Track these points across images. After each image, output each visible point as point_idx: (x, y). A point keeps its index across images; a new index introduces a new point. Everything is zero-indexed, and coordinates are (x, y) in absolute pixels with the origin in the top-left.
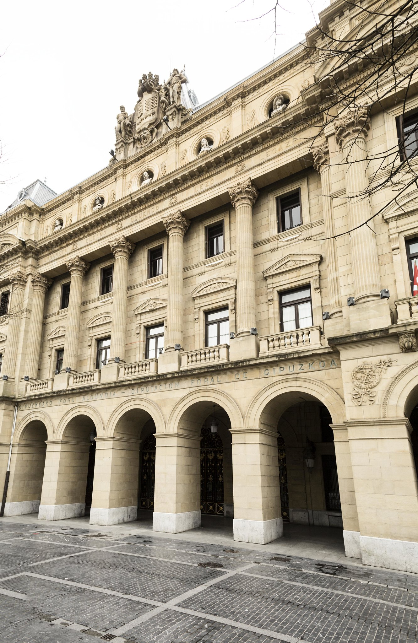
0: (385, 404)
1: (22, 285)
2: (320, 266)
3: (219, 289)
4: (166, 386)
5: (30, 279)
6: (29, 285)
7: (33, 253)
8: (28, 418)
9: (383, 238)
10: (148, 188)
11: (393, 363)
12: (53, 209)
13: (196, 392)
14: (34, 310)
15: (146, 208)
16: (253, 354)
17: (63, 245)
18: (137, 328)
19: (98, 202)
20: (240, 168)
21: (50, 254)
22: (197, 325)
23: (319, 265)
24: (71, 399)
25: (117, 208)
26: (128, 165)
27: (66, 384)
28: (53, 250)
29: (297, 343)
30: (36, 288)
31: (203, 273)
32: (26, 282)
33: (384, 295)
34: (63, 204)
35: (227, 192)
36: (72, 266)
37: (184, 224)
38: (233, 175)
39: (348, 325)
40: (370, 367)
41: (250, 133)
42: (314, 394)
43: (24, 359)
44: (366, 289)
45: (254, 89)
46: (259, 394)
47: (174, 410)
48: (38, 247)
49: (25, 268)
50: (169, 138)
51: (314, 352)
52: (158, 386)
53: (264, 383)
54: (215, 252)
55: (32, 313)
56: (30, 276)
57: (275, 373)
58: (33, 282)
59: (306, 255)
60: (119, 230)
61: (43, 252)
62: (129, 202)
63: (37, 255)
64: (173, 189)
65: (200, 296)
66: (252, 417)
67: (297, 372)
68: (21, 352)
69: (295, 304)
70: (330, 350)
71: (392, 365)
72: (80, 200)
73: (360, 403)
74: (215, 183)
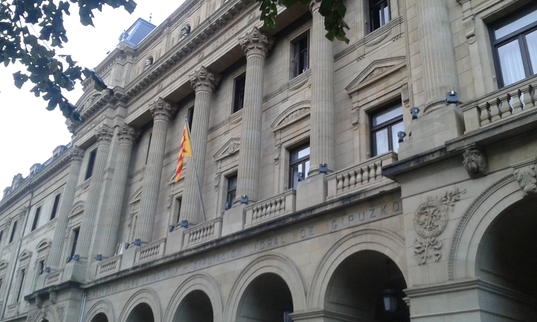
0: (452, 258)
3: (301, 117)
4: (228, 255)
5: (116, 131)
6: (115, 139)
7: (122, 101)
8: (94, 310)
9: (458, 25)
10: (224, 7)
11: (462, 196)
12: (146, 47)
14: (117, 169)
15: (226, 30)
17: (150, 87)
18: (216, 178)
19: (185, 31)
21: (138, 99)
22: (277, 167)
24: (135, 281)
27: (133, 261)
28: (140, 95)
30: (122, 141)
31: (286, 99)
32: (112, 136)
33: (452, 100)
34: (155, 40)
36: (196, 81)
37: (263, 43)
40: (434, 204)
42: (386, 252)
43: (99, 232)
44: (433, 95)
46: (325, 258)
47: (233, 289)
49: (112, 119)
51: (381, 190)
53: (331, 239)
55: (115, 172)
56: (117, 128)
57: (344, 224)
58: (119, 134)
59: (391, 59)
60: (201, 61)
61: (131, 99)
62: (207, 27)
63: (126, 103)
64: (250, 4)
65: (281, 129)
66: (317, 293)
68: (97, 223)
72: (169, 34)
73: (424, 261)
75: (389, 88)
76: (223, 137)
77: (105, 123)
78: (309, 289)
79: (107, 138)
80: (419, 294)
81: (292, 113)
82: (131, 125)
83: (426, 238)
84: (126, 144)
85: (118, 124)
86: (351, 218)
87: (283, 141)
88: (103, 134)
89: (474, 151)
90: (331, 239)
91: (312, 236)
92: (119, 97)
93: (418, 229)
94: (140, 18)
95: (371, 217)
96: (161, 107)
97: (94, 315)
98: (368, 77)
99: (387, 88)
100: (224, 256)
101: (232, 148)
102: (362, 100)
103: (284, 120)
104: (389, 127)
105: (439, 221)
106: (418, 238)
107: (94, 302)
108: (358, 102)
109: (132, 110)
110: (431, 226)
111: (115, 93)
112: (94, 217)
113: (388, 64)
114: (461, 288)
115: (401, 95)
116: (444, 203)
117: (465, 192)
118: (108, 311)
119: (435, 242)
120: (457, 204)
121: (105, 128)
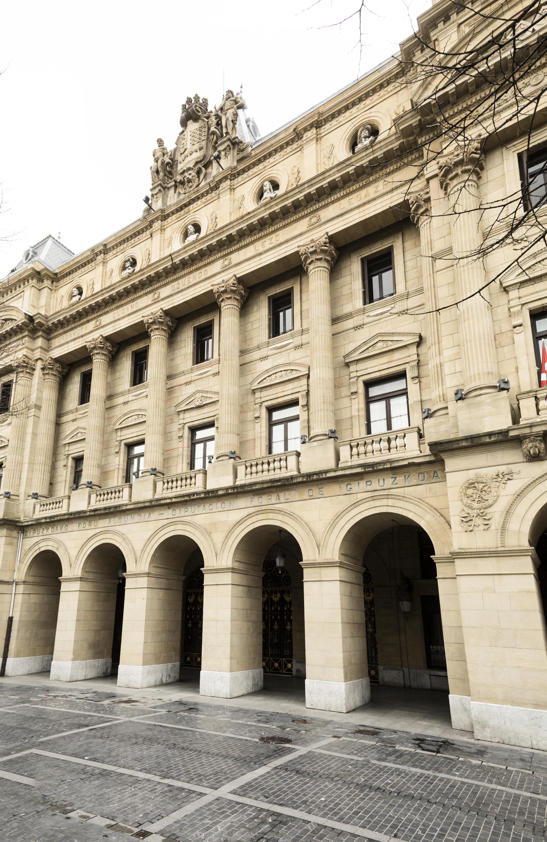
0: (503, 529)
1: (29, 373)
2: (419, 349)
4: (217, 506)
5: (39, 365)
6: (38, 373)
7: (43, 331)
8: (37, 547)
11: (515, 476)
12: (69, 273)
13: (257, 513)
16: (332, 464)
17: (83, 321)
19: (128, 264)
20: (314, 220)
23: (418, 347)
24: (93, 522)
25: (81, 308)
26: (168, 216)
29: (389, 449)
30: (47, 377)
31: (266, 358)
32: (34, 370)
34: (83, 267)
35: (298, 252)
38: (304, 229)
39: (456, 425)
40: (485, 481)
41: (327, 174)
43: (31, 470)
44: (480, 379)
45: (333, 116)
47: (227, 537)
48: (50, 323)
49: (33, 350)
50: (221, 181)
51: (410, 461)
52: (207, 506)
53: (346, 501)
54: (281, 330)
56: (39, 361)
57: (360, 488)
58: (43, 369)
59: (400, 334)
61: (56, 330)
62: (169, 264)
63: (49, 334)
64: (226, 247)
65: (262, 388)
67: (389, 487)
68: (27, 461)
69: (387, 398)
70: (432, 458)
71: (513, 478)
73: (471, 528)
74: (282, 240)
75: (393, 363)
76: (184, 388)
77: (25, 354)
78: (322, 542)
79: (28, 371)
80: (463, 556)
81: (276, 373)
82: (57, 360)
83: (474, 509)
84: (51, 382)
85: (42, 357)
86: (369, 483)
87: (263, 400)
88: (23, 366)
89: (539, 438)
90: (346, 501)
91: (322, 496)
92: (41, 327)
93: (465, 501)
94: (50, 236)
95: (392, 484)
96: (102, 346)
97: (38, 552)
98: (370, 349)
99: (392, 361)
100: (211, 507)
101: (199, 400)
102: (361, 370)
103: (265, 379)
104: (387, 399)
105: (490, 496)
106: (465, 509)
107: (36, 539)
108: (357, 371)
109: (58, 344)
110: (480, 499)
111: (36, 321)
112: (22, 455)
113: (395, 338)
114: (519, 554)
115: (405, 371)
116: (495, 480)
117: (519, 473)
118: (58, 549)
119: (484, 514)
120: (509, 482)
121: (26, 359)
